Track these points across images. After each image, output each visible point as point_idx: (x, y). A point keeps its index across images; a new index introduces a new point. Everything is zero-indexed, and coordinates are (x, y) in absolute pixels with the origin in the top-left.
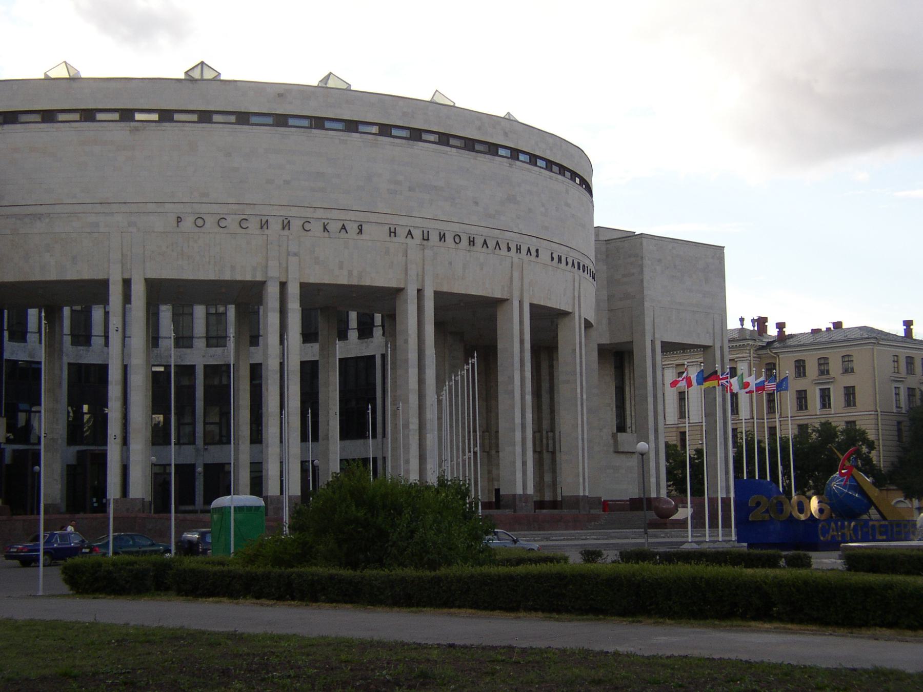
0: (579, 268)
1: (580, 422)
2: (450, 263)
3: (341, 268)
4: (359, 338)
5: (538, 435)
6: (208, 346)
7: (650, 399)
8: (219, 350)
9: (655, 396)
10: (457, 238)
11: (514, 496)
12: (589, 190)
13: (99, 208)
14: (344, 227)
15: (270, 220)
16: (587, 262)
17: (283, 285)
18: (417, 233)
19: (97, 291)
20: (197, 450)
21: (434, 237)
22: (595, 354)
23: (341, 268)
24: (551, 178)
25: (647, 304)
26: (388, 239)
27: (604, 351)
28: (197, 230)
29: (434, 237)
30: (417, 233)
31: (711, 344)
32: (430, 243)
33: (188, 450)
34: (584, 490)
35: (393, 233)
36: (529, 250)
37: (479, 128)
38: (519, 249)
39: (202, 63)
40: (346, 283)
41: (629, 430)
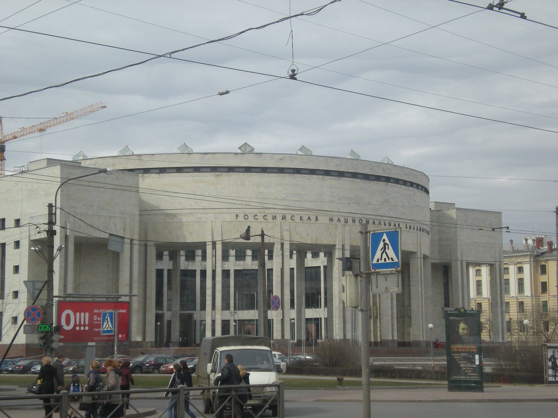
0: (420, 230)
1: (421, 305)
3: (308, 236)
4: (312, 257)
5: (406, 303)
6: (236, 260)
7: (460, 292)
8: (242, 262)
9: (463, 290)
11: (388, 340)
12: (427, 192)
13: (202, 211)
14: (309, 218)
15: (268, 215)
16: (425, 227)
18: (342, 219)
19: (202, 246)
20: (231, 313)
21: (350, 220)
22: (429, 270)
23: (308, 236)
24: (406, 189)
25: (459, 243)
26: (329, 222)
27: (434, 266)
28: (245, 220)
29: (350, 220)
30: (342, 219)
32: (348, 224)
33: (226, 312)
34: (423, 337)
35: (331, 220)
36: (395, 224)
37: (371, 169)
39: (246, 143)
40: (310, 243)
41: (451, 306)
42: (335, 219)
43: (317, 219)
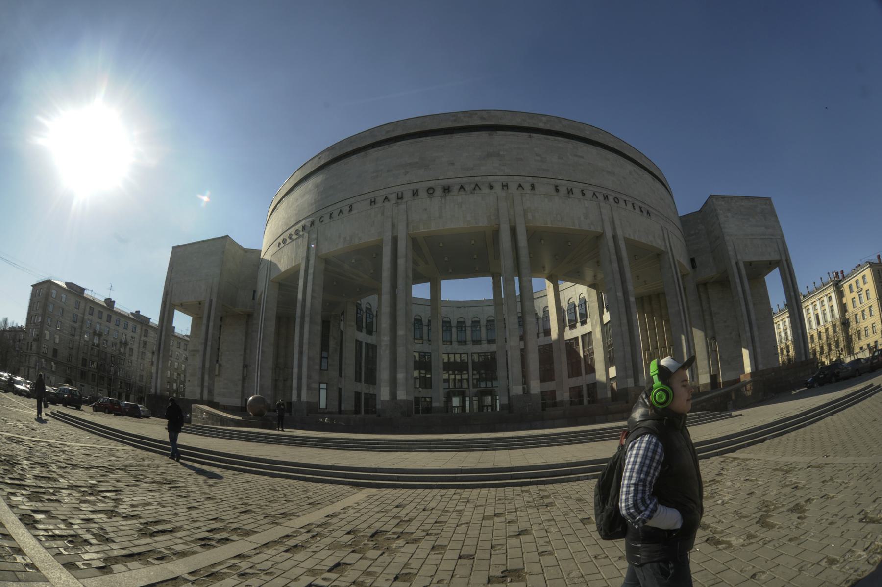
10: (431, 191)
14: (341, 211)
17: (513, 231)
18: (393, 197)
21: (408, 195)
25: (727, 238)
29: (408, 195)
31: (599, 230)
32: (404, 200)
38: (606, 198)
42: (380, 200)
43: (533, 187)
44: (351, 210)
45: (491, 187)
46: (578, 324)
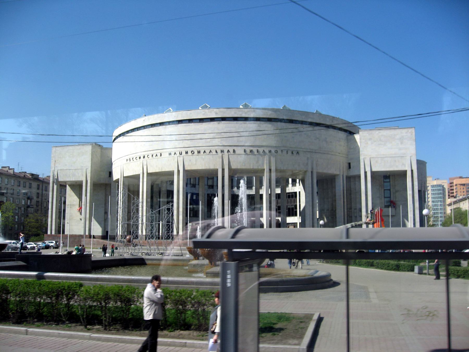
2: (190, 160)
29: (184, 153)
35: (170, 154)
42: (173, 154)
44: (161, 156)
45: (216, 152)
46: (290, 185)
